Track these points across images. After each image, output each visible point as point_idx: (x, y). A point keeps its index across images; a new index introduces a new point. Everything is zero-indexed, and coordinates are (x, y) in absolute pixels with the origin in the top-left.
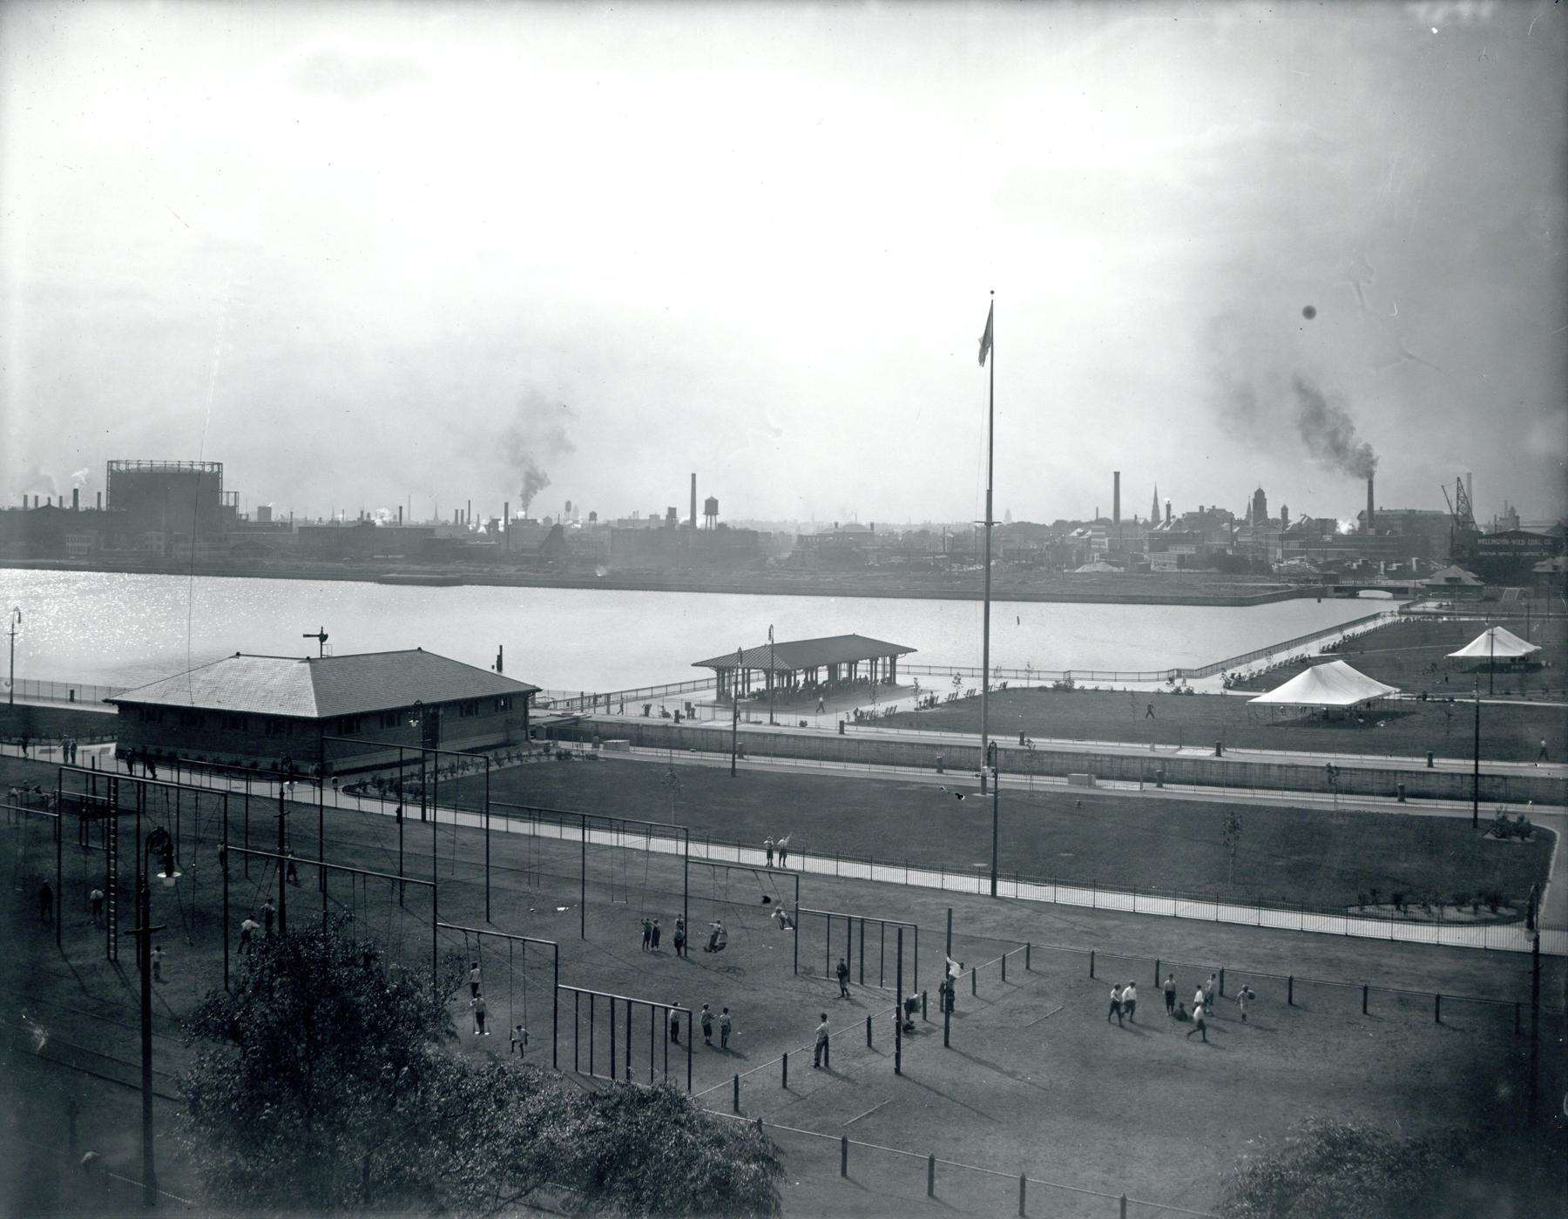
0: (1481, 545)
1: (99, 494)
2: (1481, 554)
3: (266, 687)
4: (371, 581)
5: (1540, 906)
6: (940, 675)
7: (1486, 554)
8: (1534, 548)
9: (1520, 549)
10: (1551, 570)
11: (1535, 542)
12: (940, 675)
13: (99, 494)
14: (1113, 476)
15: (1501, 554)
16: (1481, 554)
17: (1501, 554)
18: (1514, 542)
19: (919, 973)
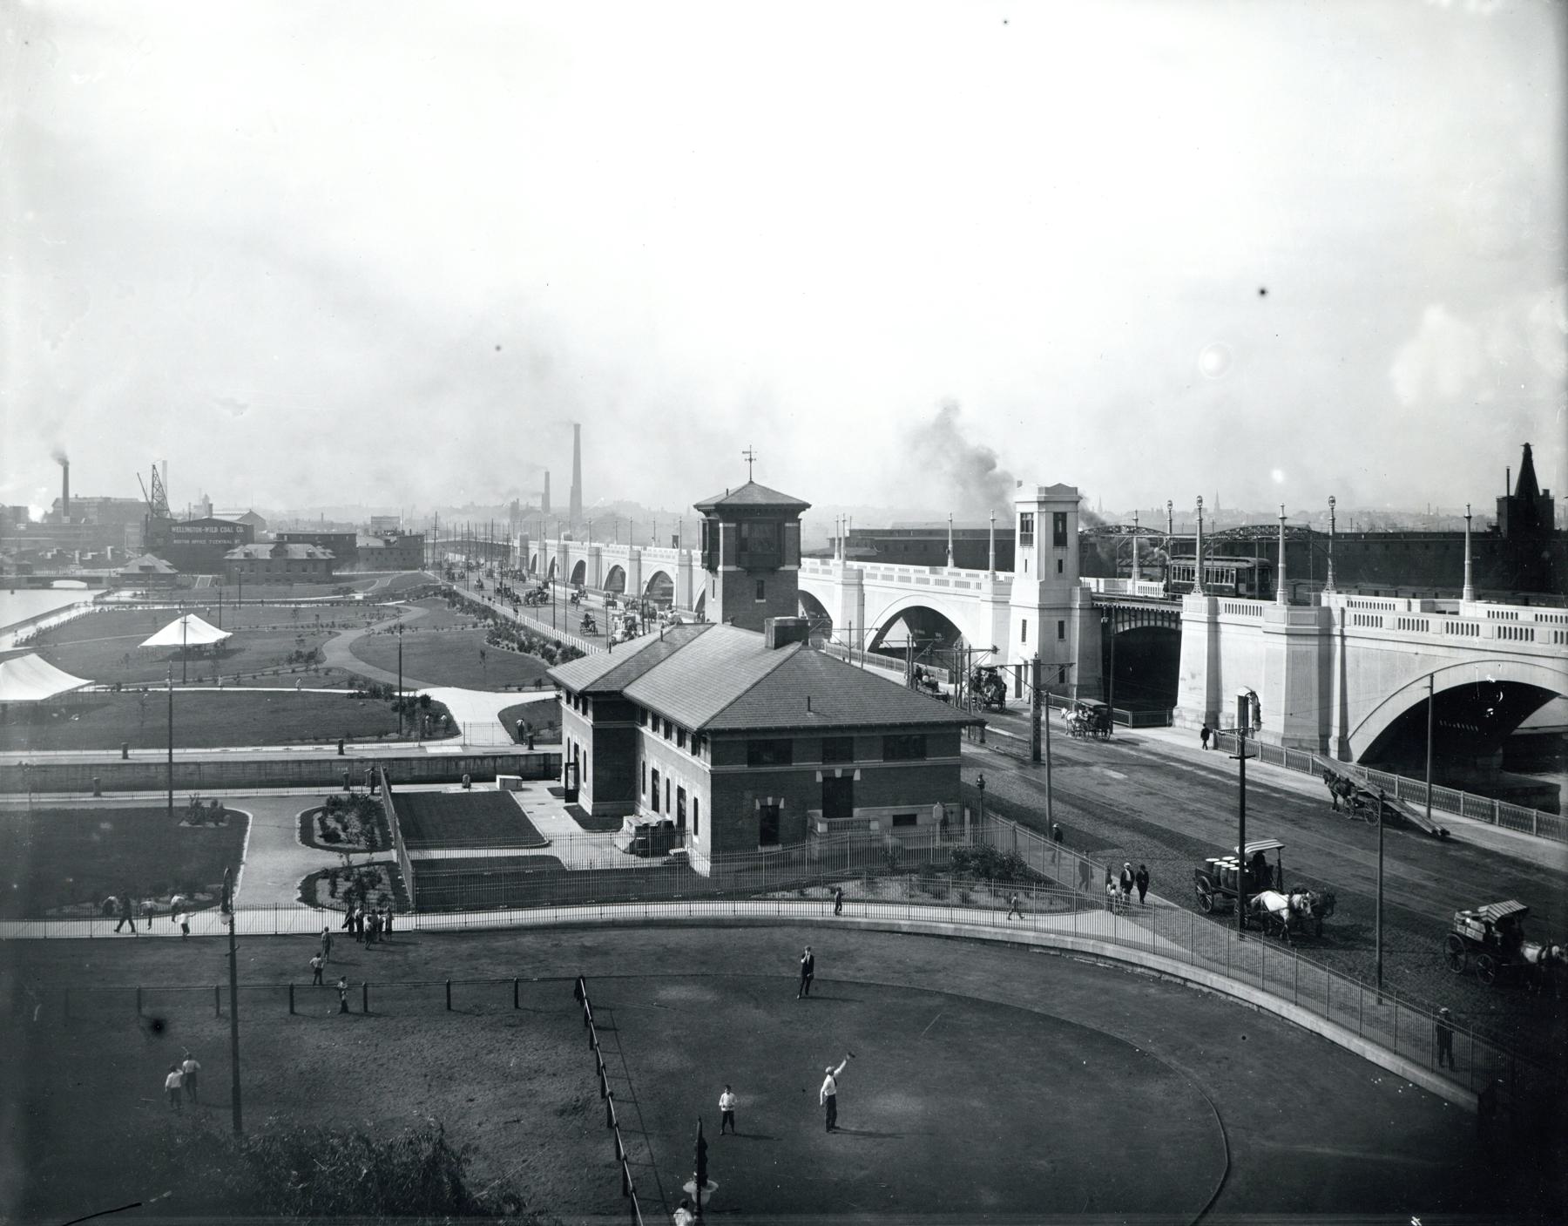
0: (175, 533)
10: (242, 557)
15: (194, 542)
17: (194, 542)
18: (207, 529)
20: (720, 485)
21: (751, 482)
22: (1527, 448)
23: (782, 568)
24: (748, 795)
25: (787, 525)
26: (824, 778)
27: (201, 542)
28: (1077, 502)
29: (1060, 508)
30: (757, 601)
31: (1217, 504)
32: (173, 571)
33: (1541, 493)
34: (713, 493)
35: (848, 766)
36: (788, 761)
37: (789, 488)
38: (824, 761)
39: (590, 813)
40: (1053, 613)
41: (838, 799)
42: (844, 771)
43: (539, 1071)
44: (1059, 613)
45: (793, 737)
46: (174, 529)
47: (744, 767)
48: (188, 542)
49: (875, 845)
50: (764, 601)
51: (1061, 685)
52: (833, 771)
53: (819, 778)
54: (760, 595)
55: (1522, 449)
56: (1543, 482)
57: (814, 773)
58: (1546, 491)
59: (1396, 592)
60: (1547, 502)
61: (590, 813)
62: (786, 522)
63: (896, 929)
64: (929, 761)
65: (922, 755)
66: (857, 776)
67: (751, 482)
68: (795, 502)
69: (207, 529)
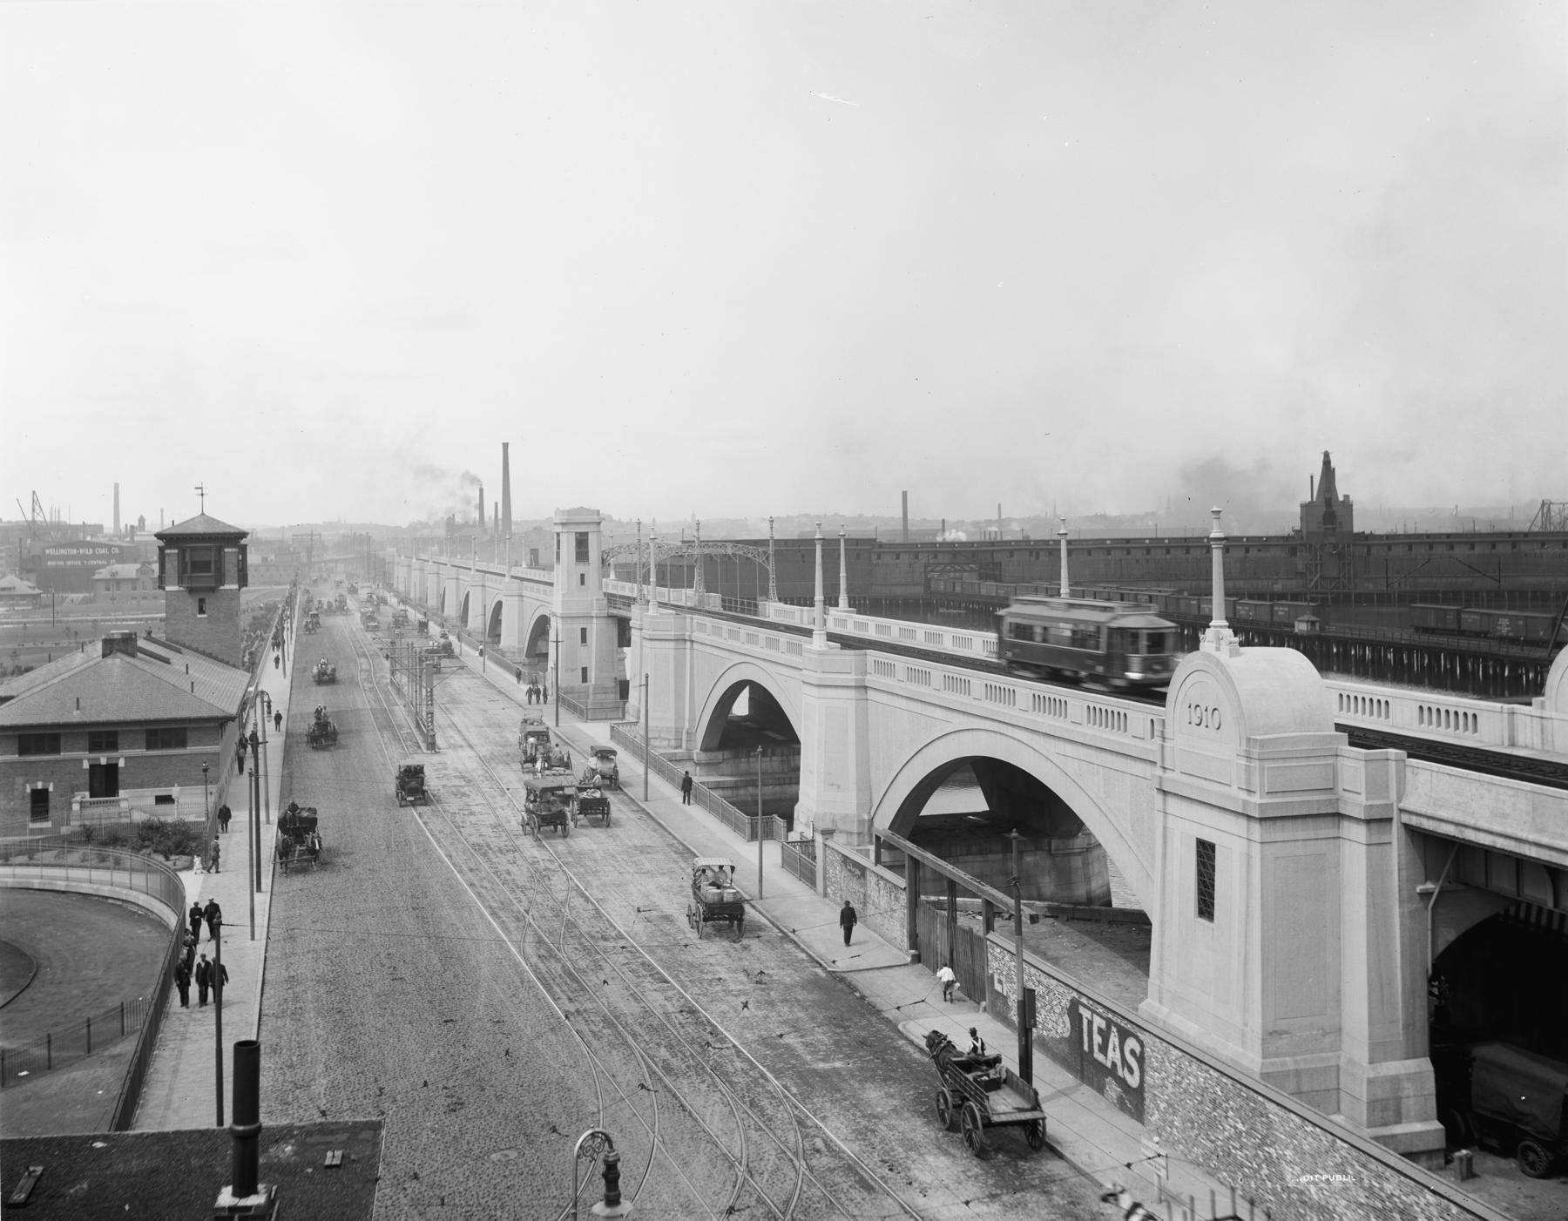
0: (49, 555)
1: (496, 504)
2: (49, 563)
3: (461, 789)
4: (186, 1132)
5: (1498, 846)
6: (1165, 843)
7: (54, 563)
8: (101, 557)
9: (89, 557)
10: (108, 577)
11: (103, 551)
12: (1165, 843)
13: (496, 504)
14: (580, 671)
15: (69, 563)
16: (49, 563)
17: (69, 563)
18: (82, 551)
19: (1293, 843)
20: (179, 513)
21: (203, 514)
22: (1327, 455)
23: (222, 588)
24: (20, 780)
25: (226, 550)
26: (90, 766)
27: (76, 563)
28: (599, 523)
29: (582, 529)
30: (199, 616)
31: (1055, 511)
32: (37, 591)
33: (1341, 498)
34: (166, 526)
35: (113, 754)
36: (58, 751)
37: (230, 516)
38: (91, 750)
39: (922, 814)
40: (577, 621)
41: (105, 782)
42: (108, 759)
43: (52, 1026)
44: (582, 621)
45: (119, 729)
46: (47, 552)
47: (16, 757)
48: (62, 563)
49: (124, 820)
50: (205, 616)
51: (584, 684)
52: (99, 759)
53: (86, 765)
54: (201, 611)
55: (1322, 456)
56: (1342, 490)
57: (80, 761)
58: (1347, 497)
59: (1122, 595)
60: (1347, 505)
61: (922, 814)
62: (225, 547)
63: (30, 886)
64: (190, 749)
65: (183, 744)
66: (121, 763)
67: (203, 514)
68: (232, 531)
69: (82, 551)
